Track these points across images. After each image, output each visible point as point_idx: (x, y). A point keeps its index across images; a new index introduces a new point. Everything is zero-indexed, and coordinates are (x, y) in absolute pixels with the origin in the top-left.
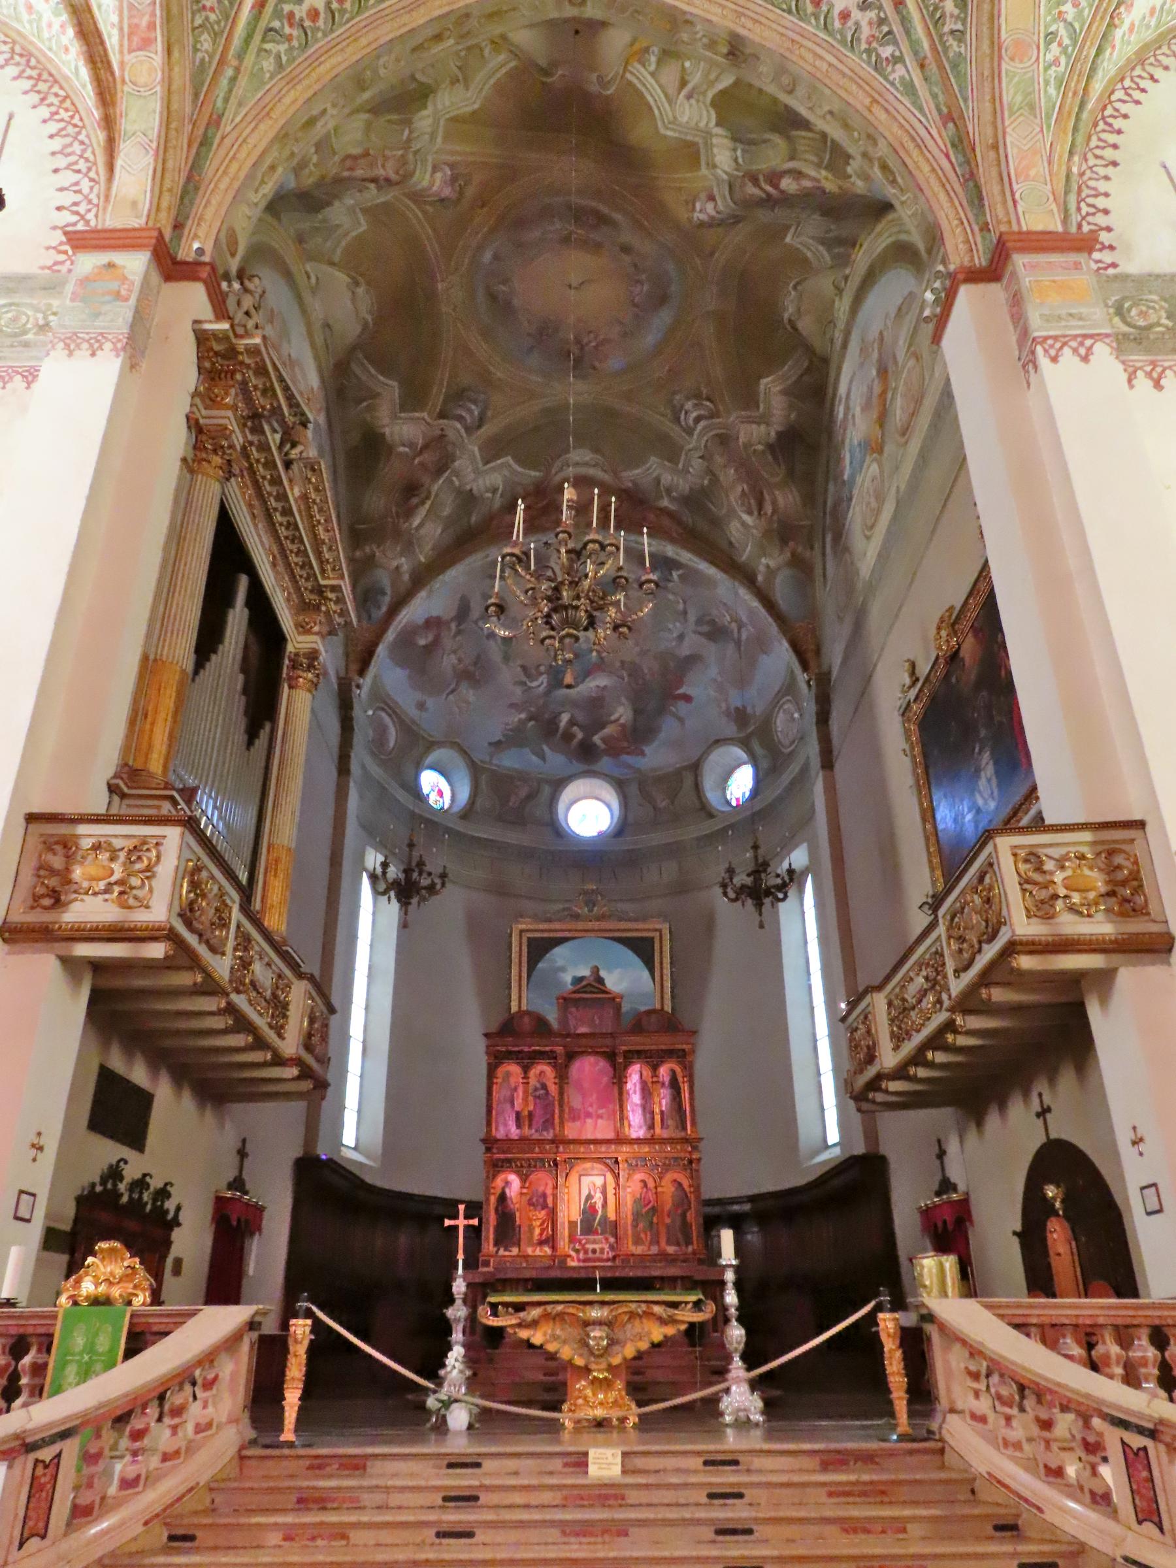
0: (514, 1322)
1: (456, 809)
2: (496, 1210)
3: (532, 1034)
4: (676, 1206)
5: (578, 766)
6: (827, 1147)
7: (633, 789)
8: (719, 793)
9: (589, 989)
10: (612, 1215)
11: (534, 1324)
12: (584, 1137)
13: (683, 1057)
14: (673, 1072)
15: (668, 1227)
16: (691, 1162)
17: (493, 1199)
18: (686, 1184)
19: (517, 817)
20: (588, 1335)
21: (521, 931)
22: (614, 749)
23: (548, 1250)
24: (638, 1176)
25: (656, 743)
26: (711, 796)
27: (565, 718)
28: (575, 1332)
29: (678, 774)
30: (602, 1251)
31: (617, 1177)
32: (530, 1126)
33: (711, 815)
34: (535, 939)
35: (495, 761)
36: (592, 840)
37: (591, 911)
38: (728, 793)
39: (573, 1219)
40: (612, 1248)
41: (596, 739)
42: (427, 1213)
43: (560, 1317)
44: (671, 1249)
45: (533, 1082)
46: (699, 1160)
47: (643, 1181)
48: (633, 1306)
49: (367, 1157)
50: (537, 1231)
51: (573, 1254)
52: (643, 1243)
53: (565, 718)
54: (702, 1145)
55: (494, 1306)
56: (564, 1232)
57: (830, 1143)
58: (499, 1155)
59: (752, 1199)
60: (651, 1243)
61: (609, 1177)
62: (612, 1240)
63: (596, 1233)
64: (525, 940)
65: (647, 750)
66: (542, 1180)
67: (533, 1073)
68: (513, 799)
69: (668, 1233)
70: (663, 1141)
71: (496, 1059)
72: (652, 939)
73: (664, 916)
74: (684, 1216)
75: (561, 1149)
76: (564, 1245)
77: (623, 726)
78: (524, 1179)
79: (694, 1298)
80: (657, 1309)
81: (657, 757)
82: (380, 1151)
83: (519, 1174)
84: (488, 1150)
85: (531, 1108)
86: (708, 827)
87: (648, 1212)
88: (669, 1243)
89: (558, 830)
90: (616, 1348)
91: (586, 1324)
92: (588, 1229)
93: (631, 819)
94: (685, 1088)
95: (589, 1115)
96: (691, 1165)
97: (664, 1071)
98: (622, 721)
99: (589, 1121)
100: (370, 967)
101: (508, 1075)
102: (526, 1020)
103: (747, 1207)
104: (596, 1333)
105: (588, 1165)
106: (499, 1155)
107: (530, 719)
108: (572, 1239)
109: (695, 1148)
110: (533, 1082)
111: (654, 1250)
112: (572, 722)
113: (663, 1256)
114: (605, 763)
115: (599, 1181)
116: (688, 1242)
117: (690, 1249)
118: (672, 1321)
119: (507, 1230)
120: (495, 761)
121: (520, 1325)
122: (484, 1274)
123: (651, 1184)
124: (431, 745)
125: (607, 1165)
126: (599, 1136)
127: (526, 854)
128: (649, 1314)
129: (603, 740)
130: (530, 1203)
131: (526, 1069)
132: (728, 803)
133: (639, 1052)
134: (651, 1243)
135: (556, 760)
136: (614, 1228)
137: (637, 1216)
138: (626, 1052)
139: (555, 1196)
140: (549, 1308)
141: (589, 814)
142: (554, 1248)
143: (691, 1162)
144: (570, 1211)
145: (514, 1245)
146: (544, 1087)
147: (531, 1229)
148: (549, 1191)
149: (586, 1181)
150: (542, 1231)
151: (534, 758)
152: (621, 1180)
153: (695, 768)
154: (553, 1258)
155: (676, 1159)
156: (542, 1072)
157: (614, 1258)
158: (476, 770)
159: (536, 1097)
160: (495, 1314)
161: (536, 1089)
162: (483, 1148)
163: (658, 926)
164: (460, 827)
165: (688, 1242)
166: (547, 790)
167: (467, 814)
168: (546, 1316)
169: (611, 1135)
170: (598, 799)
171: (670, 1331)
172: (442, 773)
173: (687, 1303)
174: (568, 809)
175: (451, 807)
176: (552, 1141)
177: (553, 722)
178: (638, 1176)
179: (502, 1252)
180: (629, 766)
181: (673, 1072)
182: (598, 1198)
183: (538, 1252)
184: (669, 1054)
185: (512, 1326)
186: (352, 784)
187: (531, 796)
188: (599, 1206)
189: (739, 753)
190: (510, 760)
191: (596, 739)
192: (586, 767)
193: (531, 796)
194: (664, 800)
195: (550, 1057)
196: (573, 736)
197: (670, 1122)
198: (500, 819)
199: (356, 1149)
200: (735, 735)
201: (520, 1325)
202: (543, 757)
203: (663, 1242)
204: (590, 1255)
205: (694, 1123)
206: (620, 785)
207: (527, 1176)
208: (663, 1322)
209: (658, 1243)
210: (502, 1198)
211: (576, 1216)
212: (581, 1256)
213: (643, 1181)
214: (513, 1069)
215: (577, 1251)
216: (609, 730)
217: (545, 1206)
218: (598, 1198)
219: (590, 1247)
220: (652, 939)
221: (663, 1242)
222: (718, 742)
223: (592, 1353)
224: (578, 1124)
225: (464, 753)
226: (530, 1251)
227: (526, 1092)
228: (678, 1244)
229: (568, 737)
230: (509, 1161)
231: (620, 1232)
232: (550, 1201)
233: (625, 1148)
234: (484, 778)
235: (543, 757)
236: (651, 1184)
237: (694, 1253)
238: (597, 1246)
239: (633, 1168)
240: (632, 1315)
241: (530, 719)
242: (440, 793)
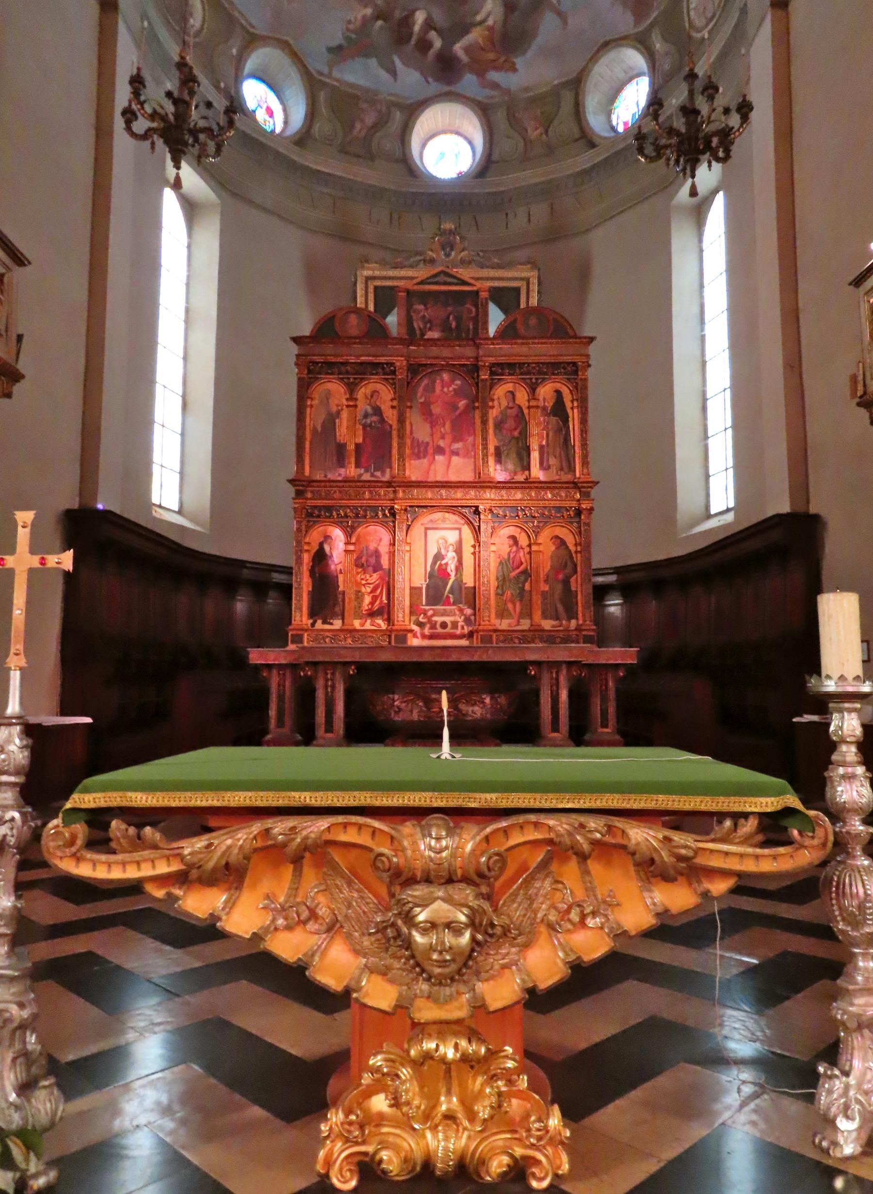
0: (163, 869)
1: (289, 132)
2: (312, 572)
3: (360, 339)
4: (556, 570)
5: (435, 87)
6: (709, 516)
7: (500, 118)
8: (602, 118)
9: (443, 278)
10: (468, 580)
11: (231, 875)
12: (431, 478)
13: (574, 371)
14: (559, 393)
15: (544, 593)
16: (579, 512)
17: (306, 558)
18: (570, 540)
19: (364, 151)
20: (409, 919)
21: (368, 279)
22: (480, 68)
23: (381, 623)
24: (506, 532)
25: (530, 54)
26: (595, 121)
27: (420, 17)
28: (359, 902)
29: (555, 93)
30: (455, 625)
31: (476, 531)
32: (358, 465)
33: (592, 145)
34: (384, 287)
35: (336, 74)
36: (451, 182)
37: (448, 255)
38: (614, 118)
39: (416, 584)
40: (467, 620)
41: (458, 48)
42: (266, 583)
43: (318, 852)
44: (547, 624)
45: (363, 406)
46: (591, 510)
47: (513, 538)
48: (559, 825)
49: (191, 520)
50: (367, 599)
51: (415, 628)
52: (510, 616)
53: (420, 17)
54: (594, 493)
55: (98, 819)
56: (402, 598)
57: (713, 512)
58: (314, 503)
59: (617, 570)
60: (521, 616)
61: (467, 531)
62: (469, 611)
63: (447, 602)
64: (371, 289)
65: (519, 62)
66: (377, 536)
67: (362, 393)
68: (358, 126)
69: (544, 604)
70: (540, 485)
71: (311, 372)
72: (517, 290)
73: (533, 264)
74: (566, 583)
75: (401, 494)
76: (402, 617)
77: (491, 29)
78: (349, 532)
79: (769, 804)
80: (640, 835)
81: (529, 73)
82: (208, 520)
83: (344, 529)
84: (299, 494)
85: (360, 440)
86: (586, 159)
87: (518, 577)
88: (545, 616)
89: (408, 167)
90: (496, 957)
91: (403, 878)
92: (436, 595)
93: (496, 156)
94: (574, 416)
95: (440, 450)
96: (579, 516)
97: (546, 391)
98: (490, 22)
99: (439, 458)
100: (187, 311)
101: (328, 395)
102: (353, 319)
103: (612, 578)
104: (433, 907)
105: (438, 515)
106: (314, 503)
107: (378, 17)
108: (414, 610)
109: (586, 495)
110: (363, 406)
111: (525, 624)
112: (429, 25)
113: (536, 633)
114: (469, 82)
115: (452, 537)
116: (571, 614)
117: (573, 623)
118: (690, 870)
119: (326, 597)
120: (336, 74)
121: (182, 878)
122: (293, 652)
123: (523, 541)
124: (252, 41)
125: (463, 516)
126: (453, 477)
127: (375, 194)
128: (609, 850)
129: (467, 50)
130: (358, 564)
131: (352, 388)
132: (613, 129)
133: (511, 365)
134: (521, 616)
135: (410, 80)
136: (471, 597)
137: (503, 581)
138: (493, 365)
139: (392, 554)
140: (279, 827)
141: (447, 149)
142: (389, 620)
143: (579, 512)
144: (413, 574)
145: (334, 615)
146: (378, 411)
147: (359, 596)
148: (384, 549)
149: (434, 536)
150: (375, 598)
151: (384, 75)
152: (483, 538)
153: (576, 84)
154: (388, 633)
155: (559, 509)
156: (375, 392)
157: (470, 635)
158: (313, 85)
159: (365, 427)
160: (99, 842)
161: (366, 416)
162: (291, 491)
163: (525, 274)
164: (296, 155)
165: (571, 614)
166: (398, 116)
167: (302, 139)
168: (272, 853)
169: (468, 476)
170: (458, 133)
171: (679, 898)
172: (272, 87)
173: (738, 817)
174: (424, 145)
175: (283, 131)
176: (389, 484)
177: (406, 21)
178: (506, 532)
179: (319, 625)
180: (495, 86)
181: (559, 393)
182: (450, 559)
183: (368, 626)
184: (553, 368)
185: (162, 880)
186: (122, 28)
187: (376, 127)
188: (451, 568)
189: (635, 58)
190: (358, 74)
191: (458, 48)
192: (447, 89)
193: (376, 127)
194: (537, 128)
195: (386, 371)
196: (428, 45)
197: (552, 461)
198: (343, 150)
199: (180, 512)
200: (632, 31)
201: (182, 878)
202: (393, 72)
203: (537, 615)
204: (439, 630)
205: (585, 463)
206: (484, 111)
207: (353, 528)
208: (650, 869)
209: (530, 616)
210: (321, 557)
211: (420, 580)
212: (427, 631)
213: (513, 538)
214: (333, 389)
215: (421, 625)
216: (475, 36)
217: (377, 568)
218: (450, 559)
219: (439, 619)
220: (517, 290)
221: (537, 615)
222: (607, 45)
223: (418, 965)
224: (425, 461)
225: (296, 57)
226: (357, 624)
227: (353, 420)
228: (557, 618)
229: (424, 45)
230: (329, 509)
231: (480, 602)
232: (385, 562)
233: (489, 494)
234: (322, 96)
235: (393, 72)
236: (523, 541)
237: (578, 629)
238: (448, 619)
239: (500, 520)
240: (557, 851)
241: (378, 17)
242: (270, 112)
